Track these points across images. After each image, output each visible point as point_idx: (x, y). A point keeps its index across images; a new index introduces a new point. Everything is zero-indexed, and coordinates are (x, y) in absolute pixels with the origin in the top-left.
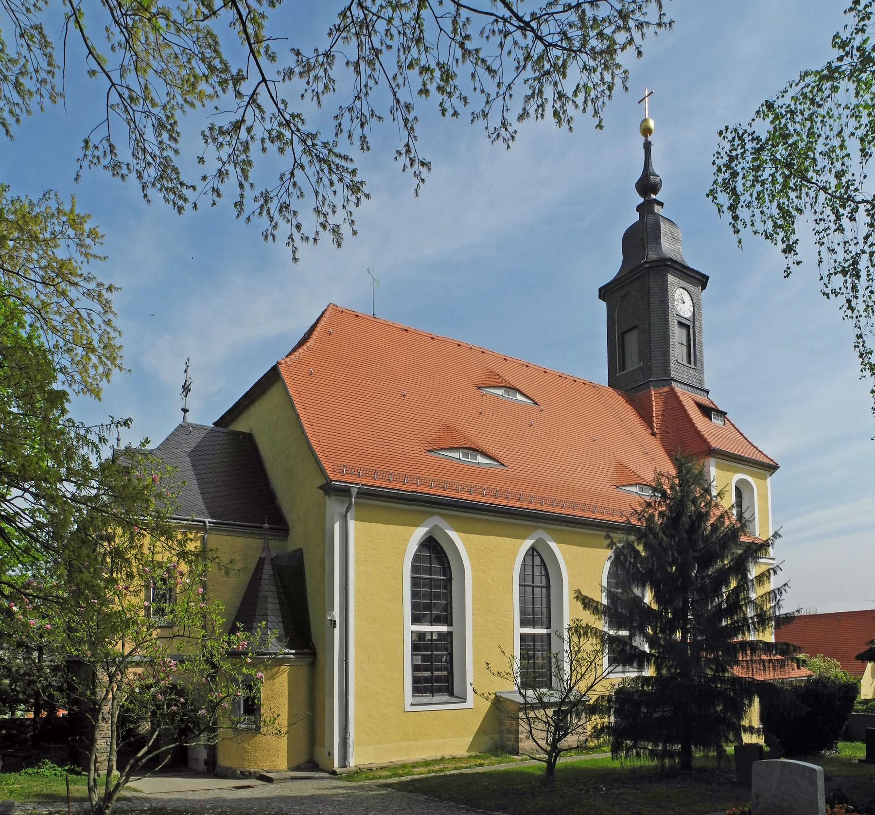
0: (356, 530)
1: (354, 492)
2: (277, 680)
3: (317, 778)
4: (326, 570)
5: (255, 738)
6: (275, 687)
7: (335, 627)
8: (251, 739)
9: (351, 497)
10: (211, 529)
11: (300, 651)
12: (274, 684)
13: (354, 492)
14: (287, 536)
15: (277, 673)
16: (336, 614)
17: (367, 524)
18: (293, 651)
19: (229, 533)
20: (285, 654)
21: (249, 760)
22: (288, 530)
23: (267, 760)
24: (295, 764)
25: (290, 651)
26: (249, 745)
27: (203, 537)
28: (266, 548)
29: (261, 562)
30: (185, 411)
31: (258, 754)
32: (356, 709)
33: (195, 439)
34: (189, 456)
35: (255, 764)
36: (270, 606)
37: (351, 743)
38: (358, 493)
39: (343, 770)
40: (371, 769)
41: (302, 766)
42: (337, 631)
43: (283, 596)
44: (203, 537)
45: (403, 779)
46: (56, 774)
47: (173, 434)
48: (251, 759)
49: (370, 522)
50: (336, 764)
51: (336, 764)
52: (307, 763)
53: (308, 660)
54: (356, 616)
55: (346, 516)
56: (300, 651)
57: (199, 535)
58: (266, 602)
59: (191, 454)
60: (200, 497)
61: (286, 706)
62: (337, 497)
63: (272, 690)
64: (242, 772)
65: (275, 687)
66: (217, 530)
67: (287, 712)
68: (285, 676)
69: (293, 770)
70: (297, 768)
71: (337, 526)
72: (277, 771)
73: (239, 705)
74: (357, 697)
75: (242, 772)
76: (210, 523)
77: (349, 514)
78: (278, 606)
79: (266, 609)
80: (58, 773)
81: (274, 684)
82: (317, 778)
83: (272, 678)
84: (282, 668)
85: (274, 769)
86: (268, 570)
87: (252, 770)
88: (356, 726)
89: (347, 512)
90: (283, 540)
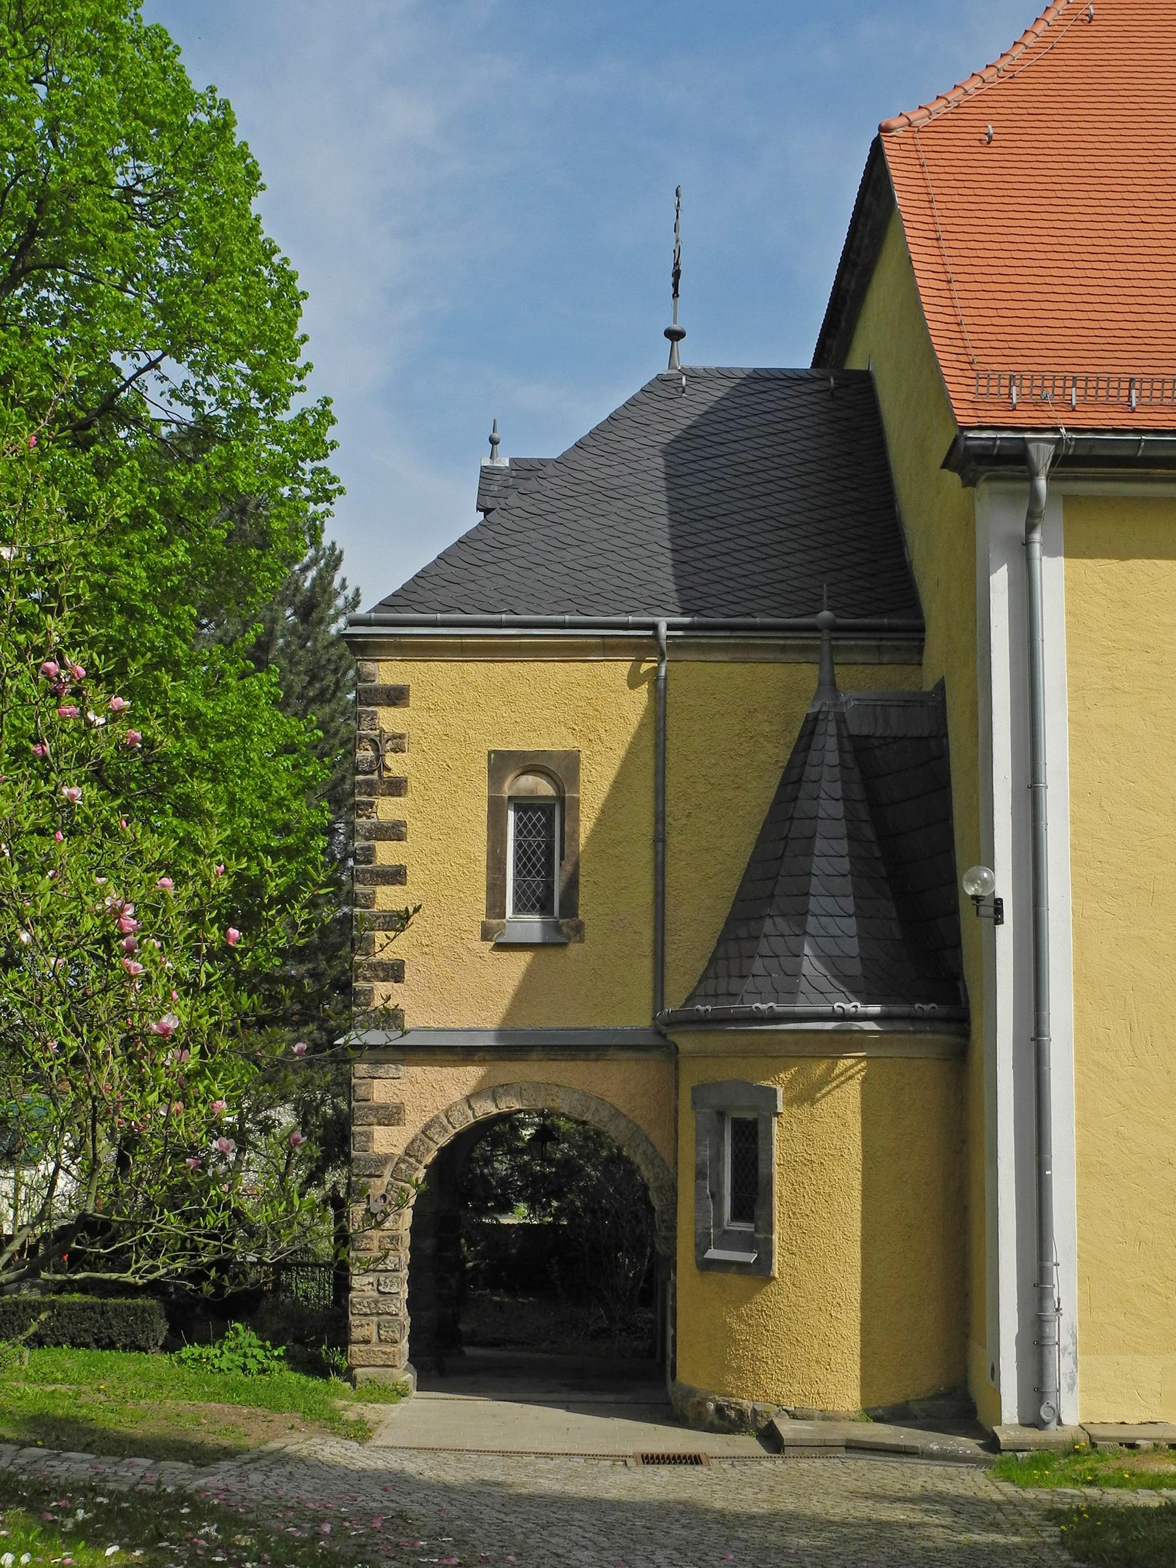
0: (1072, 587)
1: (1042, 454)
2: (824, 1106)
3: (931, 1456)
4: (980, 735)
5: (758, 1298)
6: (816, 1129)
7: (999, 920)
8: (747, 1298)
9: (1031, 477)
10: (676, 646)
11: (897, 1009)
12: (813, 1119)
13: (1042, 454)
14: (920, 650)
15: (825, 1080)
16: (1003, 884)
17: (1113, 565)
18: (875, 1009)
19: (739, 655)
20: (844, 1017)
21: (739, 1369)
22: (922, 629)
23: (792, 1375)
24: (889, 1398)
25: (861, 1009)
26: (740, 1318)
27: (656, 670)
28: (829, 685)
29: (811, 726)
30: (674, 335)
31: (765, 1352)
32: (1085, 1213)
33: (686, 413)
34: (665, 454)
35: (757, 1384)
36: (819, 865)
37: (1065, 1340)
38: (1057, 460)
39: (1032, 1435)
40: (1132, 1446)
41: (916, 1408)
42: (1005, 936)
43: (868, 832)
44: (656, 670)
45: (1114, 1496)
46: (244, 1368)
47: (632, 403)
48: (746, 1365)
49: (1122, 557)
50: (1010, 1411)
51: (1010, 1411)
52: (937, 1396)
53: (940, 1039)
54: (1081, 888)
55: (1027, 544)
56: (897, 1009)
57: (645, 667)
58: (809, 853)
59: (670, 452)
60: (667, 558)
61: (857, 1194)
62: (997, 485)
63: (807, 1136)
64: (719, 1409)
65: (816, 1129)
66: (700, 648)
67: (858, 1216)
68: (852, 1093)
69: (877, 1419)
70: (897, 1415)
71: (1000, 581)
72: (826, 1418)
73: (719, 1184)
74: (1087, 1169)
75: (719, 1409)
76: (670, 627)
77: (1037, 536)
78: (845, 865)
79: (809, 874)
80: (252, 1364)
81: (813, 1119)
82: (931, 1456)
83: (807, 1096)
84: (842, 1064)
85: (815, 1406)
86: (828, 750)
87: (747, 1404)
88: (1084, 1279)
89: (1030, 528)
90: (905, 663)
